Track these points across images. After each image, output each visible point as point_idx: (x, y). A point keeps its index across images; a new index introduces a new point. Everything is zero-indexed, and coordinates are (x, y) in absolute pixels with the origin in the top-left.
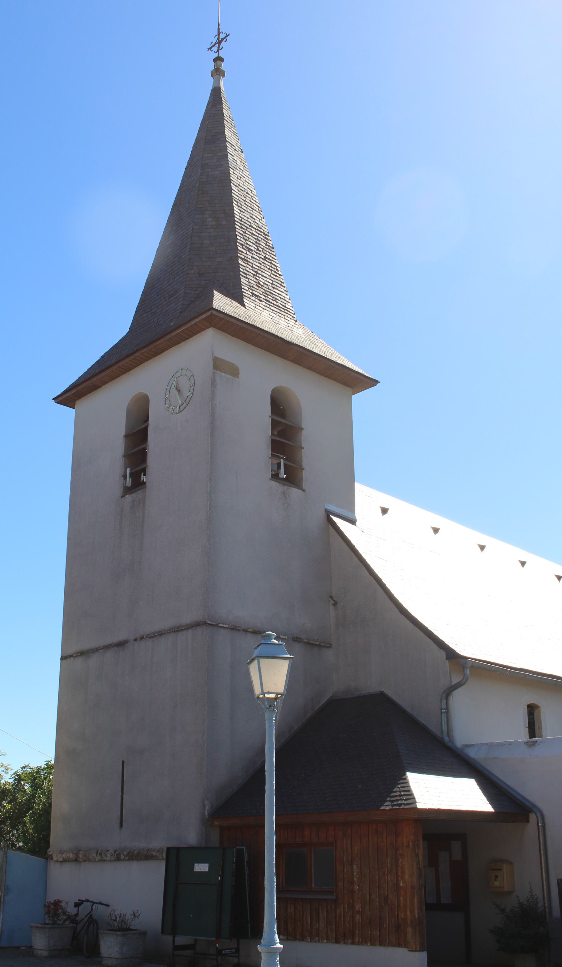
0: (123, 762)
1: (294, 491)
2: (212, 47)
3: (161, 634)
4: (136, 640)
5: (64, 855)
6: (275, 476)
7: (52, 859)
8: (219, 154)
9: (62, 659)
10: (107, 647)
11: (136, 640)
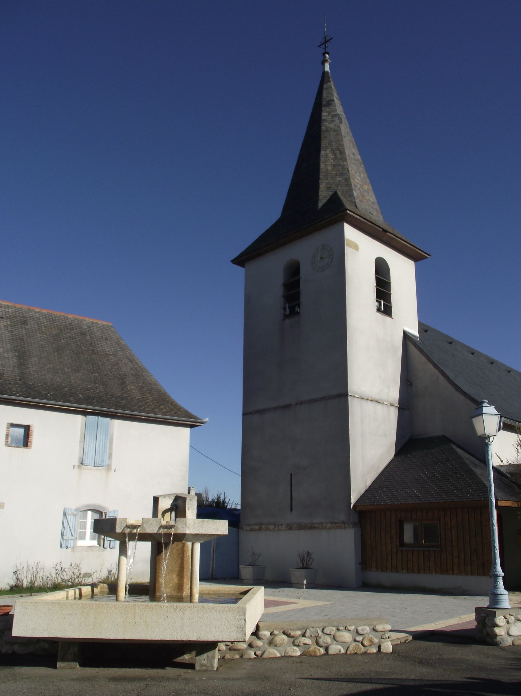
0: (291, 475)
1: (388, 318)
2: (321, 45)
3: (316, 400)
4: (297, 404)
5: (252, 527)
6: (379, 310)
7: (243, 529)
8: (332, 114)
9: (244, 414)
10: (276, 409)
11: (297, 404)
